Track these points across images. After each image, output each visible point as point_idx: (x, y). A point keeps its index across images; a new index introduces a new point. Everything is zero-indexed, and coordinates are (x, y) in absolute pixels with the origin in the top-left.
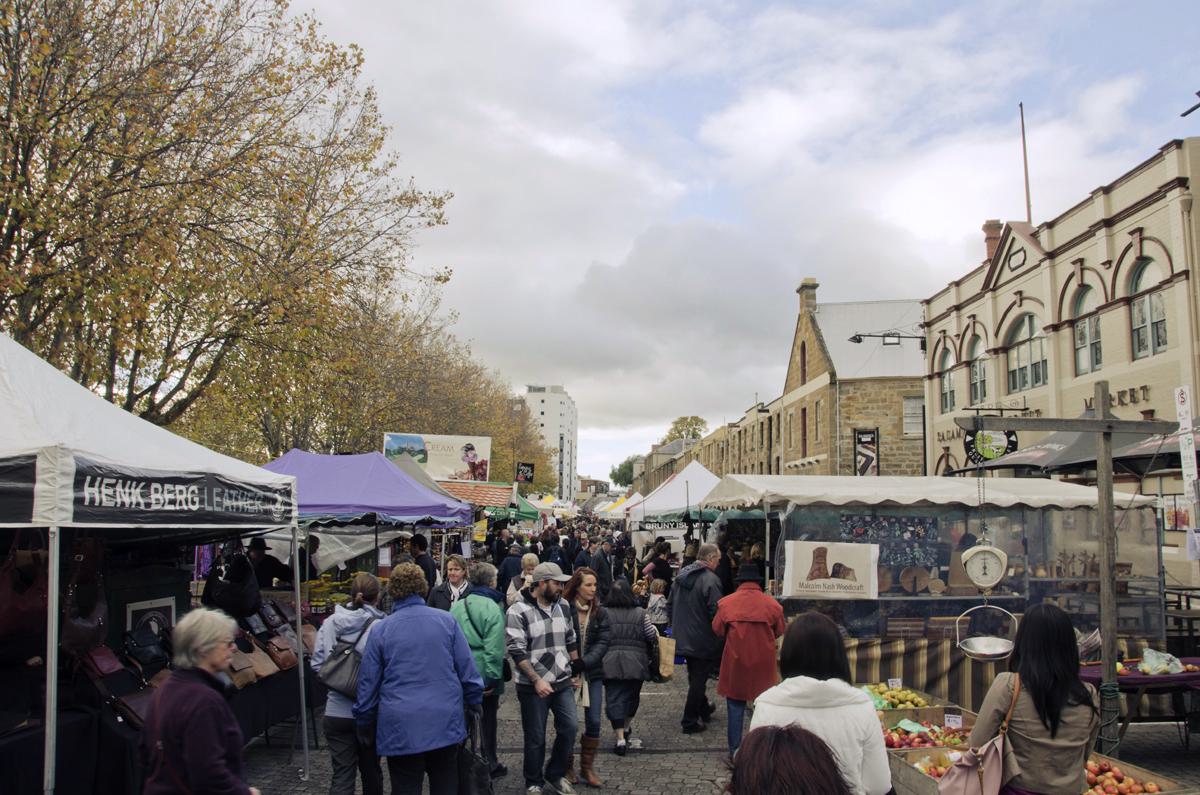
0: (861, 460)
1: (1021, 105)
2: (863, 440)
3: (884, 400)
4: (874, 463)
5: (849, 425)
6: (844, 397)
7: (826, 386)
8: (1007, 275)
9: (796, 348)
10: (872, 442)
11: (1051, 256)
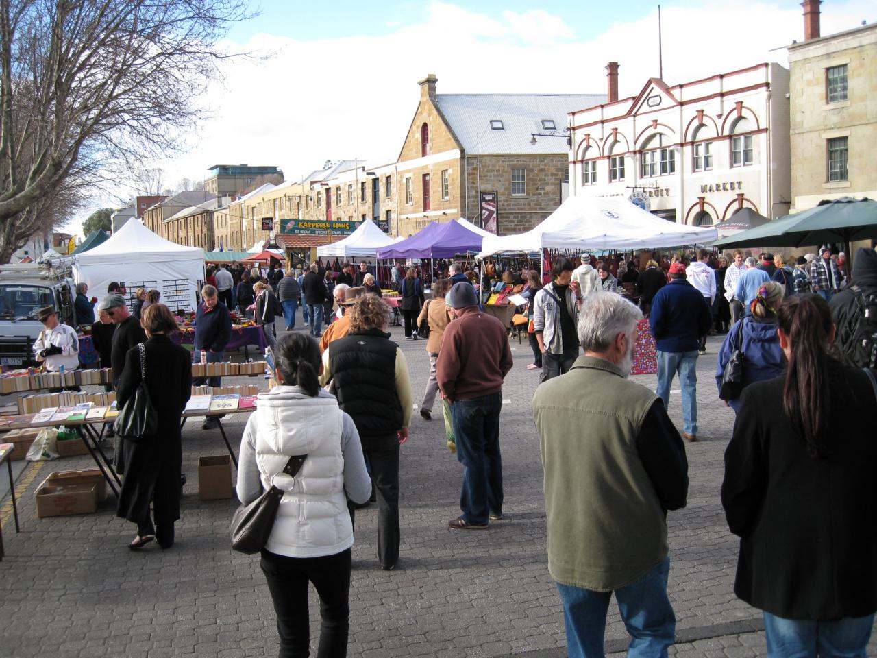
0: (486, 213)
1: (659, 6)
2: (487, 199)
3: (498, 171)
4: (495, 215)
5: (473, 188)
6: (470, 168)
7: (457, 159)
8: (645, 108)
9: (414, 128)
10: (493, 200)
11: (681, 104)
